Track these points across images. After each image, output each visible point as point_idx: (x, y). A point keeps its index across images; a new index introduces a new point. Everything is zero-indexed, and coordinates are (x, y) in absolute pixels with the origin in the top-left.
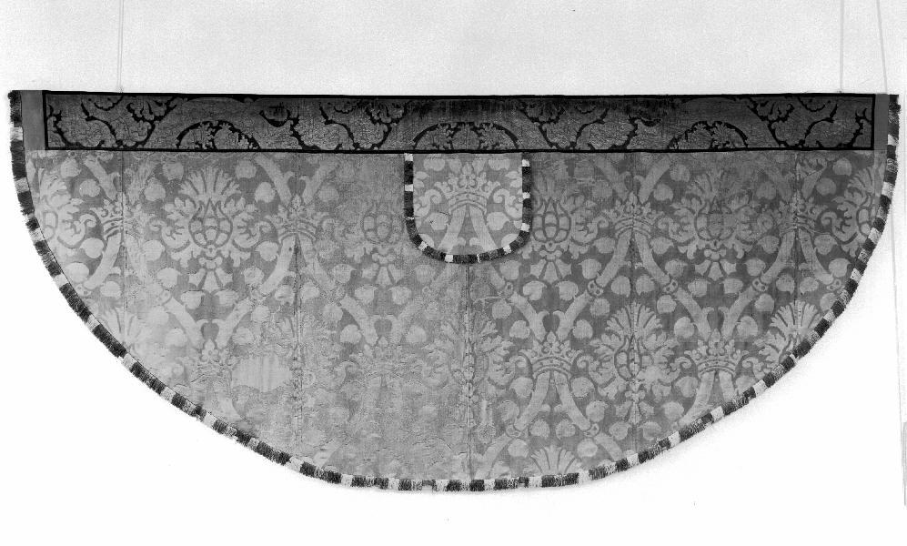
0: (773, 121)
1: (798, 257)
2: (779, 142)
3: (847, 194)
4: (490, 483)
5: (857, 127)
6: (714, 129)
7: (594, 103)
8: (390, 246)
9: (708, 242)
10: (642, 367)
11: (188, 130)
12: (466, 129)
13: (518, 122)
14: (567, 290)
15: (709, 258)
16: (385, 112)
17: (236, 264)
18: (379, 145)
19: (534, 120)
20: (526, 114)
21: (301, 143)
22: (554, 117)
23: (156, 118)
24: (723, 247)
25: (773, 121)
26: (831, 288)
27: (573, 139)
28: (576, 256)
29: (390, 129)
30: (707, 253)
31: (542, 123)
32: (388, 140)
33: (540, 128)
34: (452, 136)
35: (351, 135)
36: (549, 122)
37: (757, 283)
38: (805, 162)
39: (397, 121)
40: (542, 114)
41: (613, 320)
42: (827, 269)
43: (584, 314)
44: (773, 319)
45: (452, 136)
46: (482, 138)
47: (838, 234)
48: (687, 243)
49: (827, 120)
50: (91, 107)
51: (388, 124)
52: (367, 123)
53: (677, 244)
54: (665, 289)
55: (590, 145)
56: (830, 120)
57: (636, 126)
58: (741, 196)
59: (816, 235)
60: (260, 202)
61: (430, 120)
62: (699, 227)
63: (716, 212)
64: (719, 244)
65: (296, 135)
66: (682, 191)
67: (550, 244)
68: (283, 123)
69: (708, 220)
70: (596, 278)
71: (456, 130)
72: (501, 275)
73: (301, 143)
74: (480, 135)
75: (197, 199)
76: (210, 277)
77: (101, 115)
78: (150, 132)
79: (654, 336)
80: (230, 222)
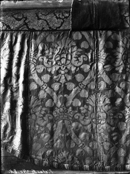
14: (71, 86)
21: (28, 27)
29: (64, 21)
35: (48, 24)
37: (80, 85)
43: (77, 96)
51: (63, 19)
60: (83, 48)
70: (82, 81)
73: (28, 27)
78: (62, 23)
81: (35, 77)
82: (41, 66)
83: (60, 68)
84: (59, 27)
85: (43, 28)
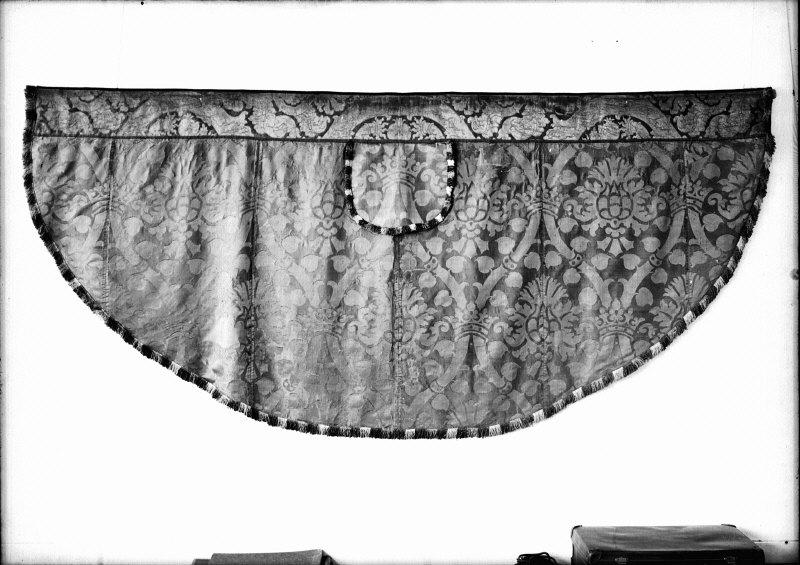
0: (675, 115)
1: (687, 232)
2: (682, 134)
3: (587, 184)
4: (410, 431)
5: (547, 121)
6: (413, 124)
7: (511, 99)
8: (620, 222)
9: (609, 221)
10: (550, 332)
11: (362, 124)
12: (399, 122)
13: (448, 115)
15: (610, 235)
16: (328, 106)
17: (637, 234)
18: (322, 135)
19: (460, 113)
20: (659, 108)
21: (254, 131)
22: (478, 111)
23: (337, 113)
24: (622, 225)
25: (675, 115)
26: (574, 263)
27: (496, 130)
28: (492, 234)
30: (608, 231)
31: (467, 117)
32: (331, 130)
33: (466, 121)
34: (387, 127)
36: (473, 116)
38: (692, 149)
39: (338, 114)
40: (466, 109)
41: (526, 291)
42: (714, 244)
44: (666, 290)
45: (387, 127)
46: (413, 130)
47: (723, 213)
48: (590, 222)
49: (724, 113)
50: (74, 100)
52: (312, 114)
53: (580, 222)
54: (570, 263)
55: (510, 135)
56: (727, 113)
57: (551, 120)
58: (637, 181)
59: (704, 214)
61: (370, 113)
62: (600, 208)
63: (614, 194)
64: (619, 223)
65: (250, 124)
66: (586, 175)
67: (471, 224)
68: (238, 114)
69: (608, 201)
71: (391, 122)
72: (426, 249)
73: (254, 131)
74: (412, 127)
75: (603, 181)
76: (616, 242)
77: (288, 110)
78: (329, 125)
79: (561, 304)
80: (200, 200)
81: (558, 241)
82: (713, 216)
83: (608, 225)
84: (118, 130)
85: (288, 134)
